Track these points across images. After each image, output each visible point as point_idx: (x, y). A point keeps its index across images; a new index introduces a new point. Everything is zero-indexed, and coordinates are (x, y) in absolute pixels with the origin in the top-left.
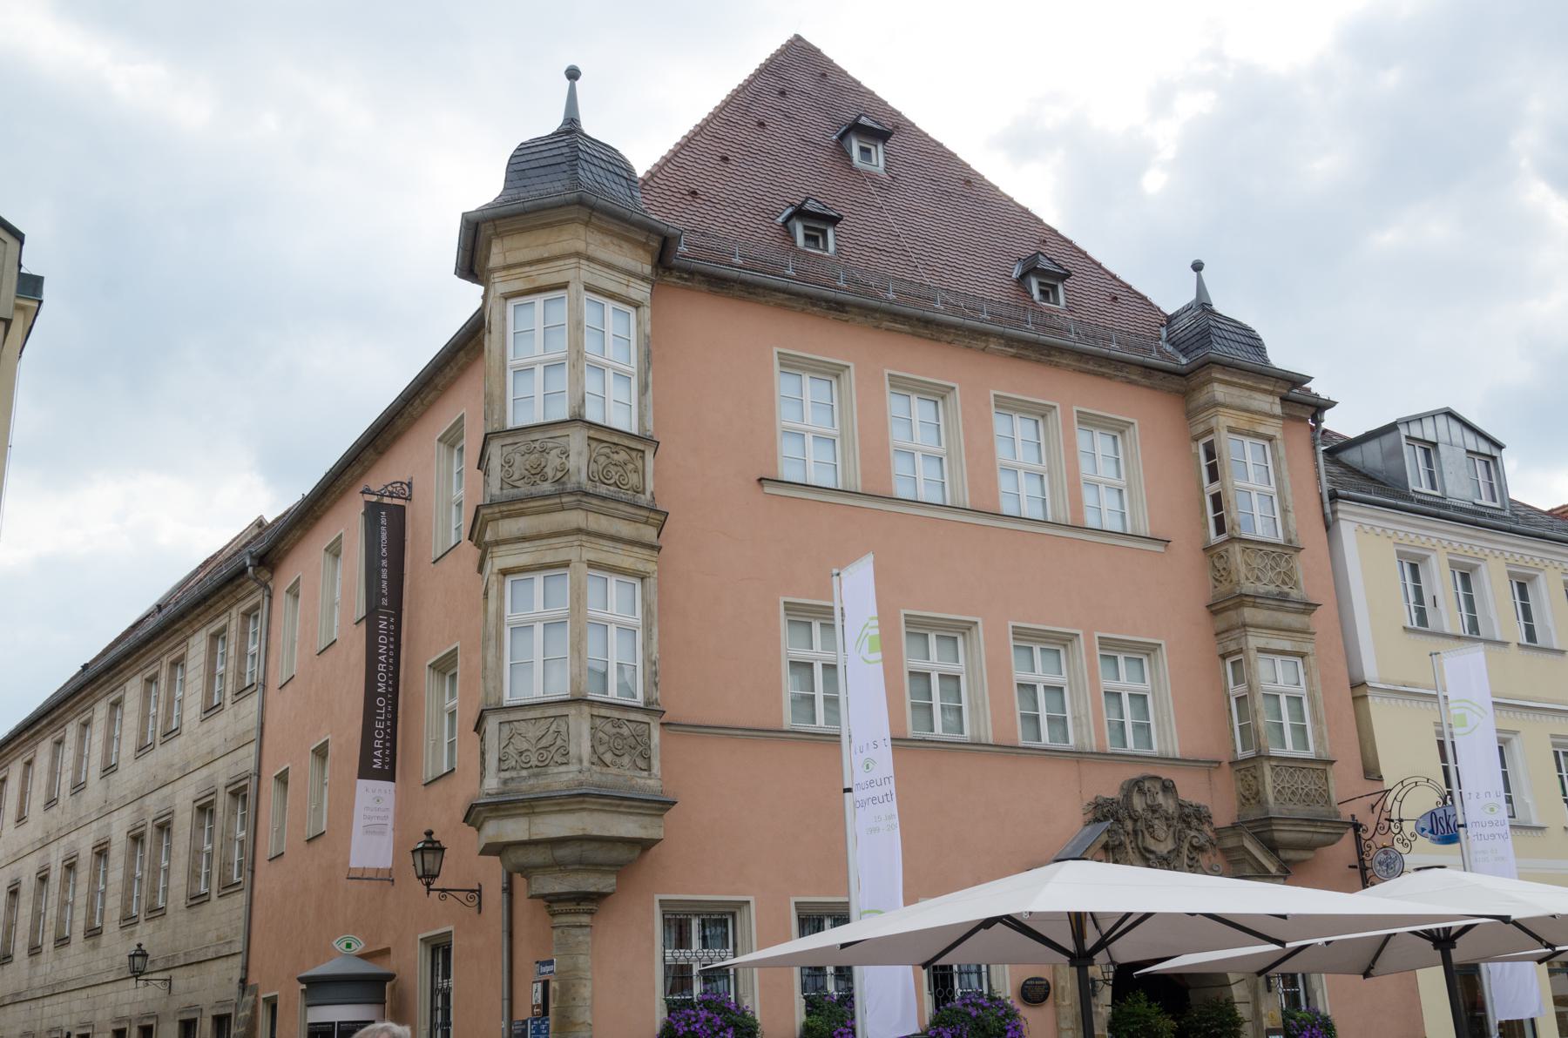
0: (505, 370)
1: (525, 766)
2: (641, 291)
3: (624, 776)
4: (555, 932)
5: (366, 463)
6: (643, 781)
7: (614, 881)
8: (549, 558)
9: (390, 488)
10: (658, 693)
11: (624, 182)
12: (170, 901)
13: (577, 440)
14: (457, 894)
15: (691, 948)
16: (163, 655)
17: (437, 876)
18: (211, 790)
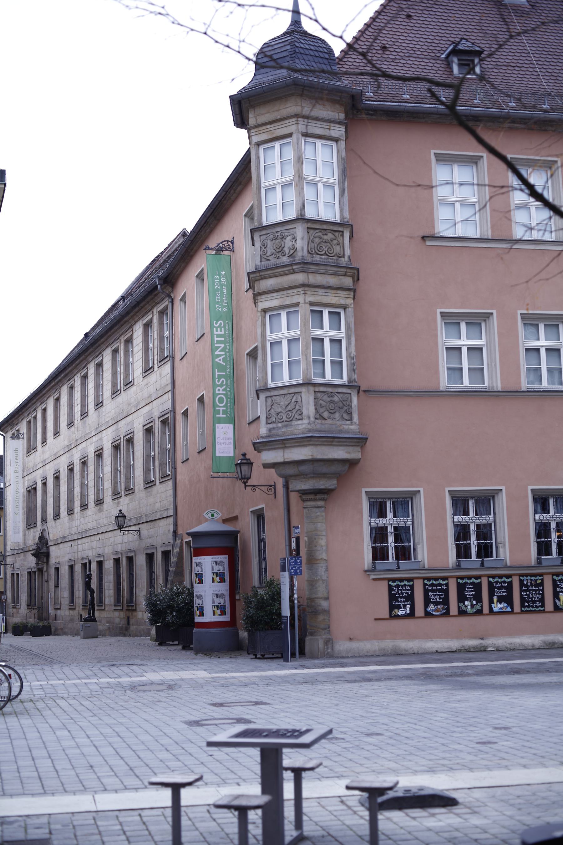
0: (260, 188)
1: (280, 421)
2: (338, 131)
3: (335, 424)
4: (305, 510)
5: (212, 226)
6: (347, 427)
7: (336, 482)
8: (288, 301)
9: (221, 245)
10: (356, 376)
11: (326, 61)
12: (136, 484)
13: (300, 231)
14: (262, 488)
15: (386, 517)
16: (121, 336)
17: (250, 478)
18: (152, 420)
